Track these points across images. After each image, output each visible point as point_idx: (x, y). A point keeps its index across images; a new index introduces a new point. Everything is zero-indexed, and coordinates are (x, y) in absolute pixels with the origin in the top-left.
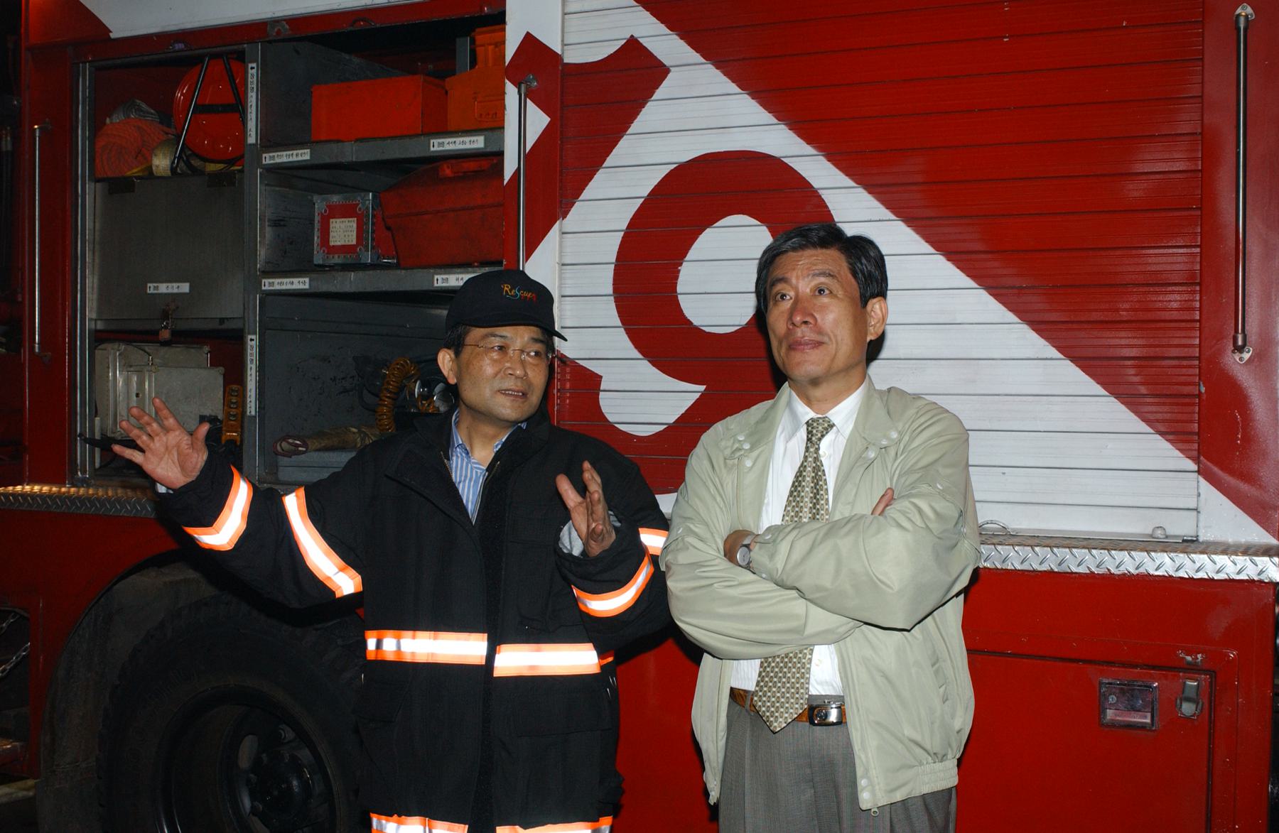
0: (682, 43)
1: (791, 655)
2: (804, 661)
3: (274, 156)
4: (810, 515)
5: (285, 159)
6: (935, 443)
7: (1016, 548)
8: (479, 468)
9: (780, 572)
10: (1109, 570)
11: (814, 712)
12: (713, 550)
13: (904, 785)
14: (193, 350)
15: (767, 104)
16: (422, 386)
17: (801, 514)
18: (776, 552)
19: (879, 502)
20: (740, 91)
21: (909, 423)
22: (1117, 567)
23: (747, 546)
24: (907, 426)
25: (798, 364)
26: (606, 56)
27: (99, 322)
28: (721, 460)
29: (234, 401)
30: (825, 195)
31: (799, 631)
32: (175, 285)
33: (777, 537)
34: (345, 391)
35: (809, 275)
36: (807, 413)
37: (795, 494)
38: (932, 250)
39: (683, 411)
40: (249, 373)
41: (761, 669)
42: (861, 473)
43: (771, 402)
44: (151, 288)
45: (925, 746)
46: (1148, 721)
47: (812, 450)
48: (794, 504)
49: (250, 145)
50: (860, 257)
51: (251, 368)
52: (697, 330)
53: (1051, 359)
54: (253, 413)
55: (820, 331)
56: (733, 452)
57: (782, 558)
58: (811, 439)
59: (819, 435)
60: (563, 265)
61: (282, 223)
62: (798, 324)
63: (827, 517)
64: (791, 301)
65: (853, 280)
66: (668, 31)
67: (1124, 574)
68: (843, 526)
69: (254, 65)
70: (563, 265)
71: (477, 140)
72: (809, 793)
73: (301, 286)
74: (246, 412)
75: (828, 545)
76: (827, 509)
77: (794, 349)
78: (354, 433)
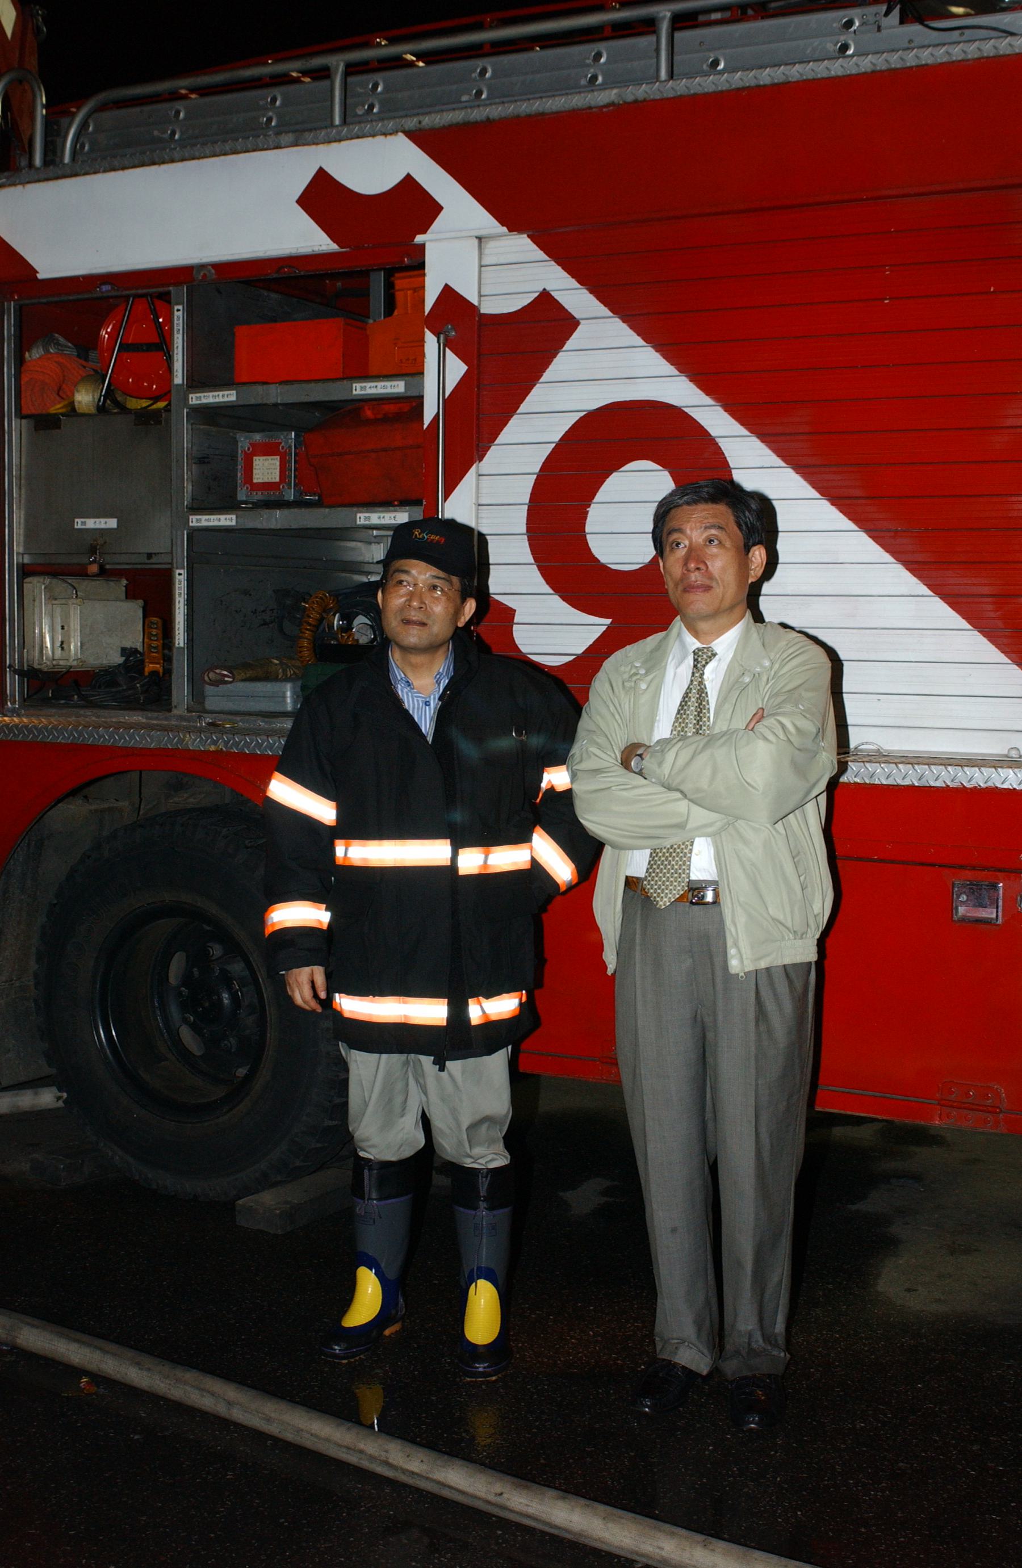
0: (591, 297)
1: (675, 846)
2: (685, 851)
3: (200, 397)
4: (694, 730)
5: (211, 400)
6: (800, 671)
7: (882, 765)
9: (666, 777)
10: (962, 784)
11: (695, 891)
12: (610, 759)
13: (768, 955)
14: (112, 583)
15: (671, 356)
16: (341, 618)
17: (686, 729)
18: (663, 761)
19: (751, 719)
20: (644, 344)
21: (780, 653)
22: (969, 782)
23: (640, 755)
24: (778, 656)
25: (692, 602)
26: (520, 307)
27: (26, 556)
28: (620, 684)
29: (154, 633)
30: (723, 444)
31: (681, 826)
32: (103, 520)
33: (665, 748)
34: (265, 624)
35: (701, 527)
36: (694, 644)
37: (682, 712)
38: (818, 496)
39: (591, 642)
40: (177, 606)
41: (651, 859)
43: (664, 633)
44: (79, 523)
45: (786, 924)
46: (994, 916)
47: (697, 675)
48: (680, 720)
49: (177, 385)
50: (744, 512)
51: (179, 602)
52: (604, 568)
53: (923, 596)
54: (182, 645)
56: (631, 677)
57: (670, 762)
58: (697, 659)
59: (704, 663)
60: (479, 505)
61: (206, 460)
63: (708, 732)
64: (686, 549)
65: (738, 532)
66: (578, 286)
67: (976, 787)
68: (719, 739)
69: (180, 307)
70: (479, 505)
71: (398, 385)
72: (689, 961)
73: (228, 523)
74: (174, 644)
75: (708, 753)
76: (708, 726)
77: (688, 591)
78: (276, 665)
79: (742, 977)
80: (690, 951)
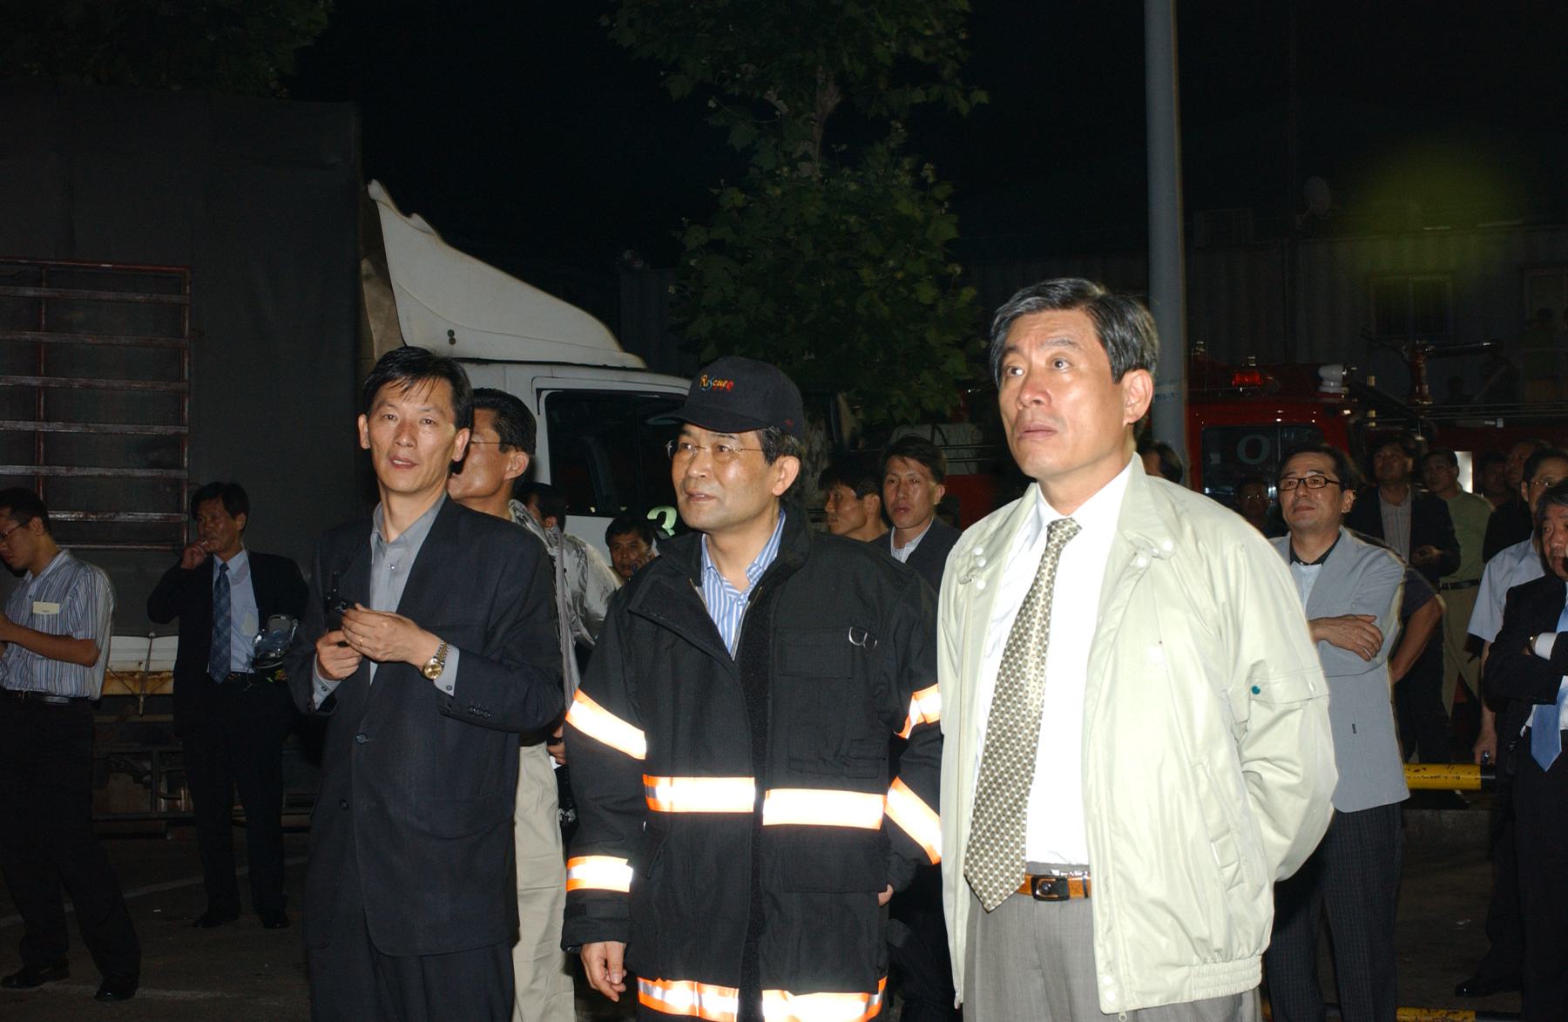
8: (732, 593)
42: (1130, 589)
55: (1054, 415)
62: (1027, 403)
72: (1040, 982)
79: (1123, 1017)
80: (1040, 967)
